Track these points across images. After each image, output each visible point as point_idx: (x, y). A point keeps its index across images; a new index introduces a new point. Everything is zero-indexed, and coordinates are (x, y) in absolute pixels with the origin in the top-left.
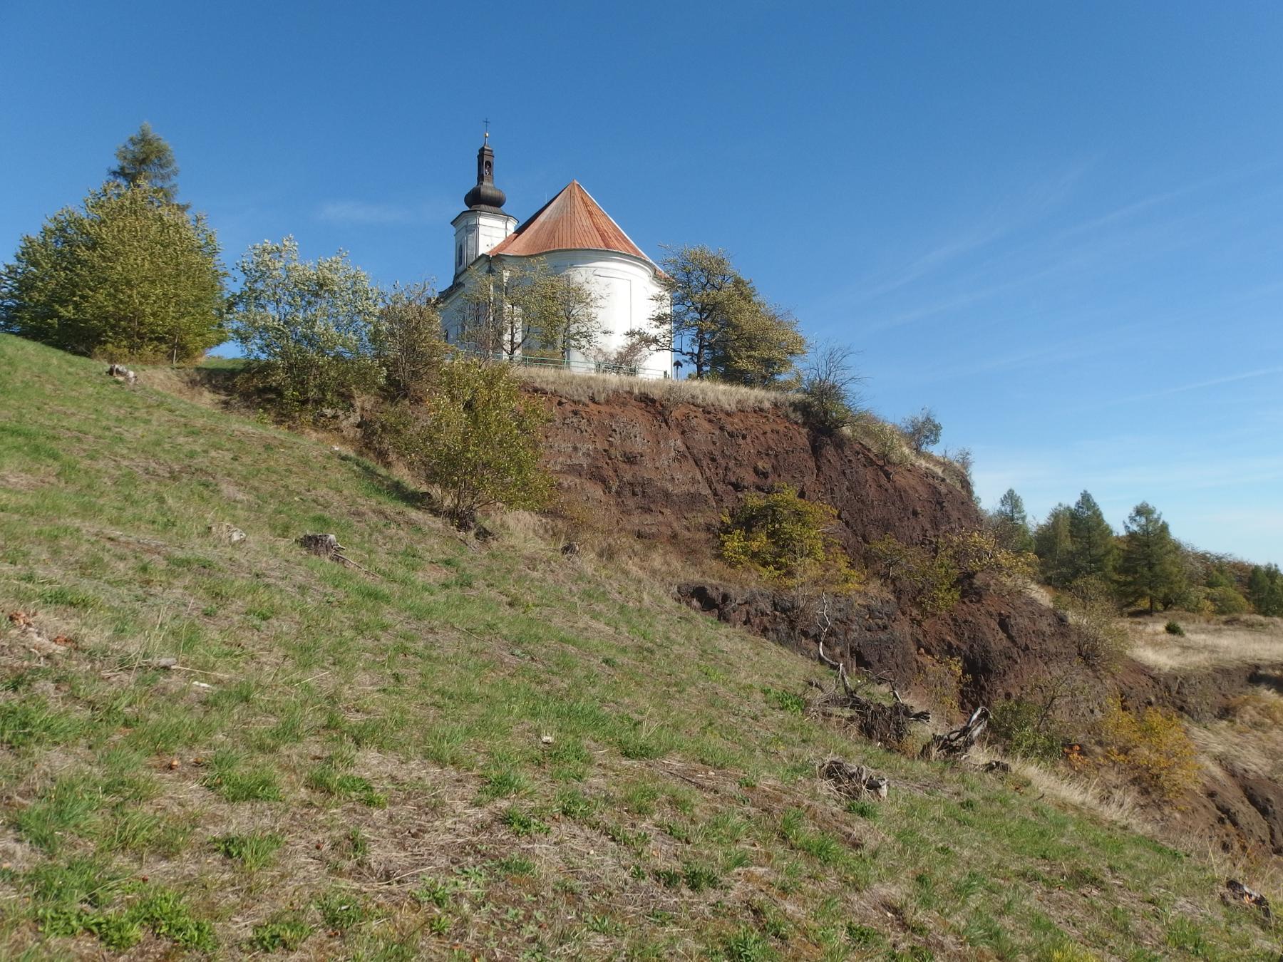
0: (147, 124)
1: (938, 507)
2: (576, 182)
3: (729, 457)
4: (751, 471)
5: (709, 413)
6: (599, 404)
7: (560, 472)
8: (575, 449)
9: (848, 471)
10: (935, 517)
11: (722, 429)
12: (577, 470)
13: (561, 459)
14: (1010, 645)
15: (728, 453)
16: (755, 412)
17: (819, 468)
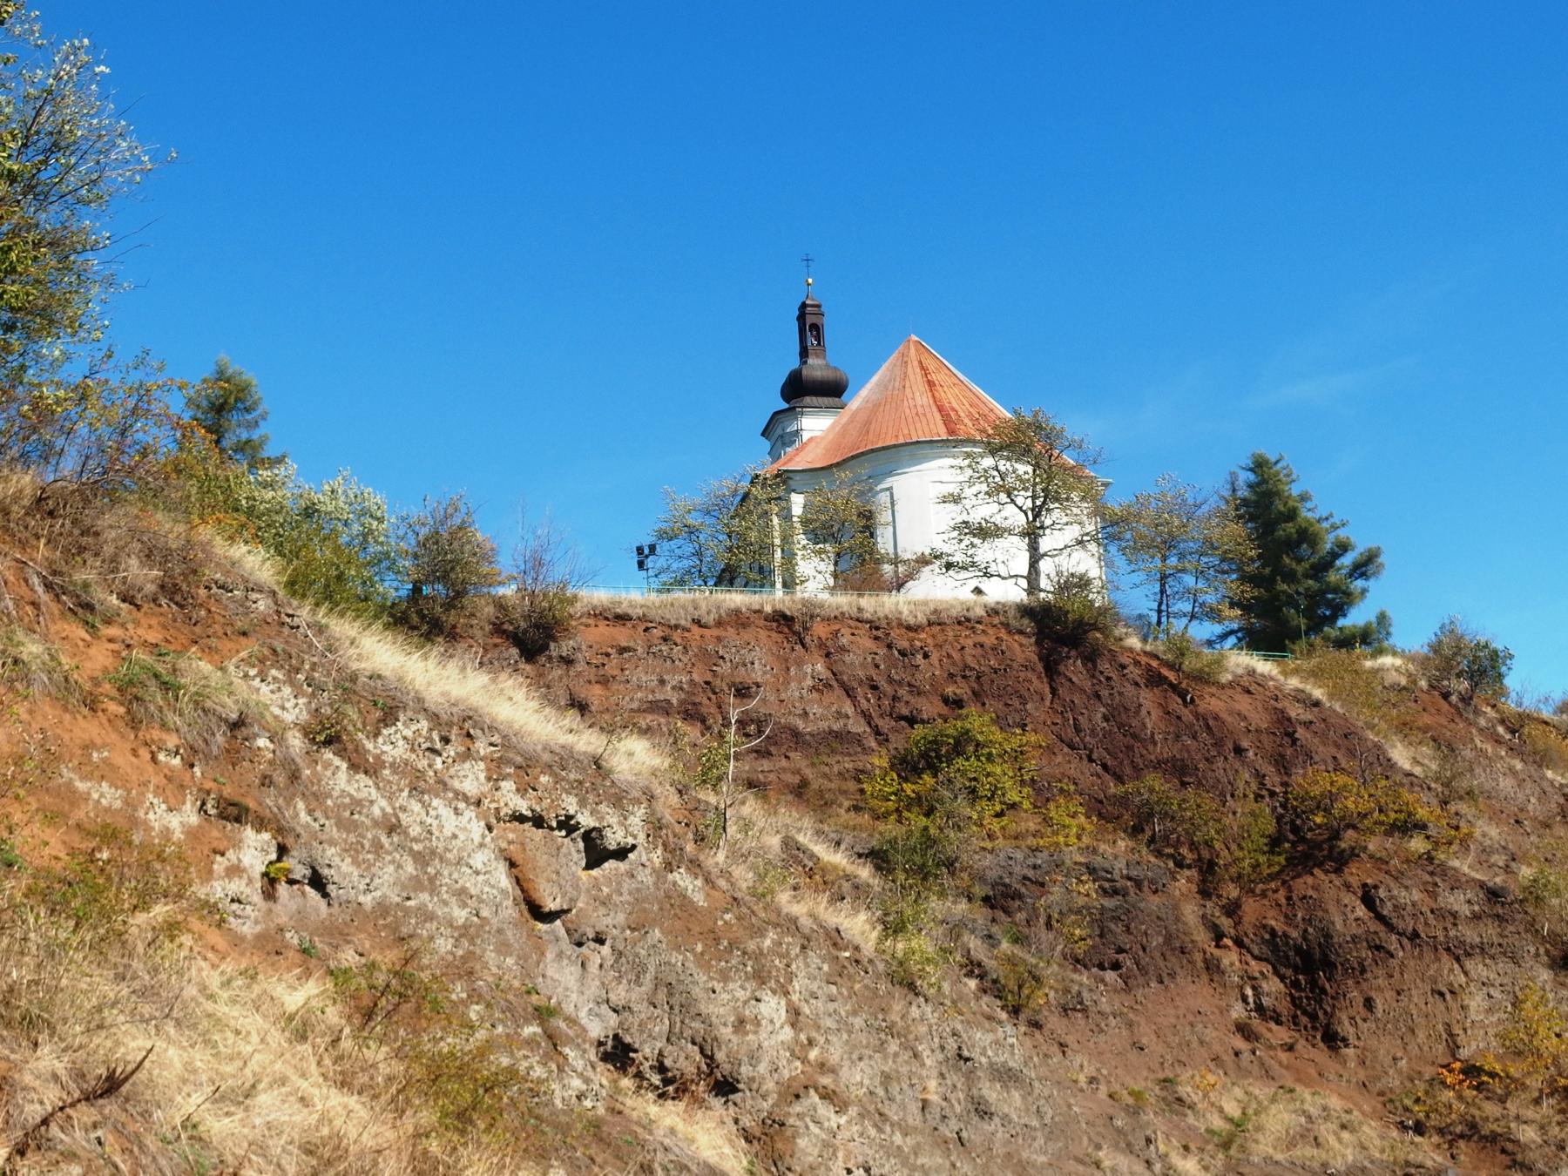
0: (224, 357)
1: (1287, 740)
2: (914, 338)
3: (900, 683)
4: (937, 701)
5: (877, 628)
6: (706, 627)
7: (639, 710)
8: (662, 682)
9: (1105, 693)
10: (1282, 756)
11: (889, 646)
12: (663, 708)
13: (639, 695)
14: (1381, 928)
15: (896, 677)
16: (959, 623)
17: (1054, 691)
